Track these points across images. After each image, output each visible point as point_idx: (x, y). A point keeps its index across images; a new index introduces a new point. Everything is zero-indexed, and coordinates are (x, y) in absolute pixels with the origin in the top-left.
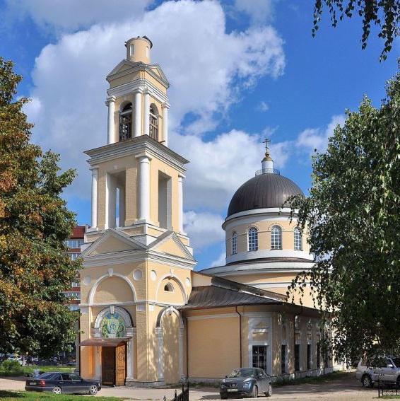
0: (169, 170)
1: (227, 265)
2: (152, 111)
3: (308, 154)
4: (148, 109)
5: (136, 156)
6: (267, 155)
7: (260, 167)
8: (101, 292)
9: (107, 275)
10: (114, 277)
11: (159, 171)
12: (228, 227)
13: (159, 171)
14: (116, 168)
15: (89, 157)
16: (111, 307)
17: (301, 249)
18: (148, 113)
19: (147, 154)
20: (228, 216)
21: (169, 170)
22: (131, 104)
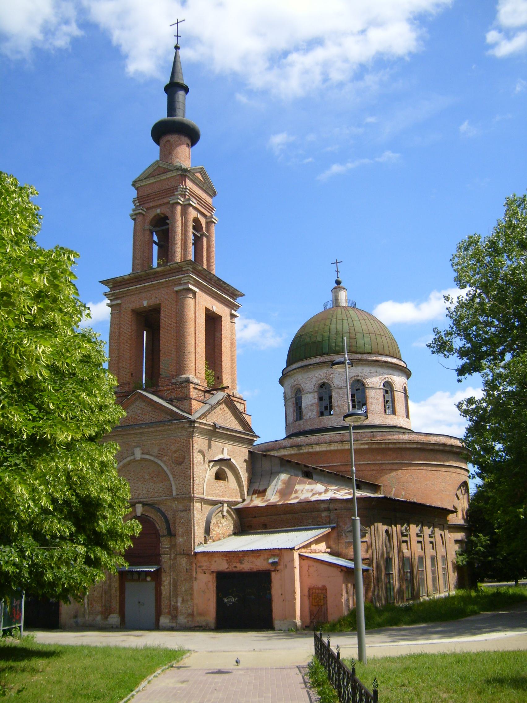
0: (218, 308)
1: (288, 437)
2: (194, 228)
3: (502, 513)
4: (191, 224)
5: (176, 289)
6: (338, 283)
7: (329, 297)
8: (245, 464)
9: (132, 457)
10: (143, 459)
11: (206, 307)
12: (289, 382)
13: (206, 307)
14: (145, 304)
15: (107, 289)
16: (137, 505)
17: (394, 413)
18: (191, 230)
19: (191, 287)
20: (288, 366)
21: (218, 308)
22: (166, 218)
